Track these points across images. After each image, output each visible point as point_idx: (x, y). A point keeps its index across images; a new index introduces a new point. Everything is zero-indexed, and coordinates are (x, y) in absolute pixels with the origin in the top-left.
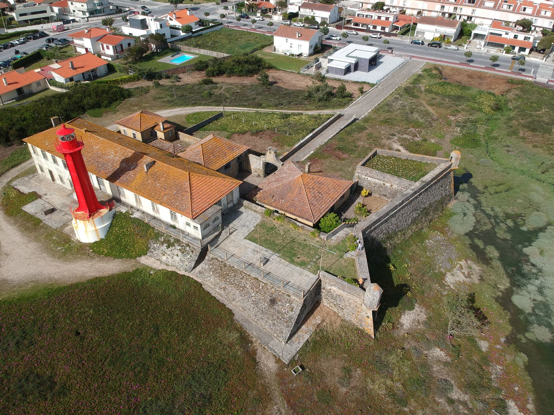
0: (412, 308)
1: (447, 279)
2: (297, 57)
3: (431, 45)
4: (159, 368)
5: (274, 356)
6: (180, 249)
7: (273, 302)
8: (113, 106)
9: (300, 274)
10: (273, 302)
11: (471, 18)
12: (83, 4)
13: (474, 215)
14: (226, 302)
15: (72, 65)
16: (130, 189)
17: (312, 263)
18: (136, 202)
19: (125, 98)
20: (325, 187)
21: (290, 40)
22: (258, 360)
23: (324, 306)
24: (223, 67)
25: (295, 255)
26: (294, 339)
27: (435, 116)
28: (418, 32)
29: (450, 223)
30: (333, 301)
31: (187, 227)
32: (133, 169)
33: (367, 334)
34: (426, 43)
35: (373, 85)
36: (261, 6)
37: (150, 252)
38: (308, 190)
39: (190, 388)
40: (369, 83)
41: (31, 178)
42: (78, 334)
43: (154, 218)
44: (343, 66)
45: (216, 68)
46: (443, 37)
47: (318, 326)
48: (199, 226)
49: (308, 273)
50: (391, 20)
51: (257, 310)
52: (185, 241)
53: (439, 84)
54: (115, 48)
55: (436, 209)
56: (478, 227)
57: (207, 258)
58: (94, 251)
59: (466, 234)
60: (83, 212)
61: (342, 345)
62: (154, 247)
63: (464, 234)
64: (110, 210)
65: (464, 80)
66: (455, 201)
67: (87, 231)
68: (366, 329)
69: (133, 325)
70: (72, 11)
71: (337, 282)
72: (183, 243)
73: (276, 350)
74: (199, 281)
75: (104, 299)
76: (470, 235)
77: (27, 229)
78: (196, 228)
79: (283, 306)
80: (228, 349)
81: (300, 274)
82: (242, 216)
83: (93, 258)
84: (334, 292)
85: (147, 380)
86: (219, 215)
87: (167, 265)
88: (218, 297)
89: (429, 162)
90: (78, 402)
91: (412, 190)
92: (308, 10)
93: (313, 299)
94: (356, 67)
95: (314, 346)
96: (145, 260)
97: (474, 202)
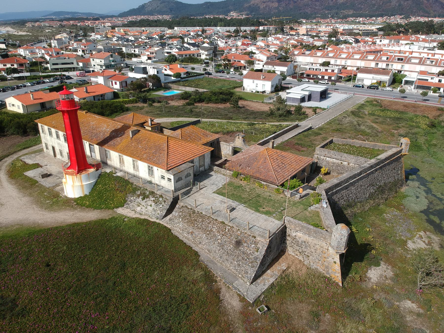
0: (378, 265)
1: (409, 245)
2: (261, 93)
3: (370, 87)
4: (120, 298)
5: (239, 295)
6: (154, 200)
7: (238, 243)
8: (113, 116)
9: (265, 220)
10: (238, 243)
11: (401, 72)
12: (101, 60)
13: (426, 198)
14: (193, 245)
15: (86, 90)
16: (116, 151)
17: (276, 213)
18: (121, 162)
19: (123, 111)
20: (288, 160)
21: (256, 81)
22: (221, 298)
23: (289, 255)
24: (203, 97)
25: (260, 206)
26: (259, 281)
27: (380, 129)
28: (358, 80)
29: (405, 202)
30: (298, 248)
31: (162, 181)
32: (121, 136)
33: (334, 282)
34: (366, 87)
35: (324, 109)
36: (234, 65)
37: (127, 204)
38: (272, 160)
39: (150, 319)
40: (320, 108)
41: (37, 155)
42: (48, 265)
43: (134, 176)
44: (299, 97)
45: (197, 97)
46: (380, 83)
47: (284, 271)
48: (172, 177)
49: (274, 220)
50: (336, 71)
51: (223, 251)
52: (159, 193)
53: (380, 110)
54: (121, 84)
55: (390, 189)
56: (431, 206)
57: (177, 206)
58: (77, 204)
59: (421, 212)
60: (73, 170)
61: (309, 291)
62: (131, 200)
63: (419, 211)
64: (97, 170)
65: (401, 108)
66: (407, 187)
67: (74, 186)
68: (333, 276)
69: (101, 260)
70: (93, 66)
71: (302, 226)
72: (157, 194)
73: (240, 290)
74: (169, 227)
75: (78, 238)
76: (425, 212)
77: (24, 188)
78: (169, 180)
79: (248, 247)
80: (191, 286)
81: (265, 220)
82: (212, 178)
83: (76, 209)
84: (300, 238)
85: (107, 309)
86: (191, 172)
87: (141, 214)
88: (185, 240)
89: (380, 149)
90: (34, 324)
91: (369, 164)
92: (270, 66)
93: (278, 245)
94: (310, 98)
95: (280, 290)
96: (121, 211)
97: (425, 189)
